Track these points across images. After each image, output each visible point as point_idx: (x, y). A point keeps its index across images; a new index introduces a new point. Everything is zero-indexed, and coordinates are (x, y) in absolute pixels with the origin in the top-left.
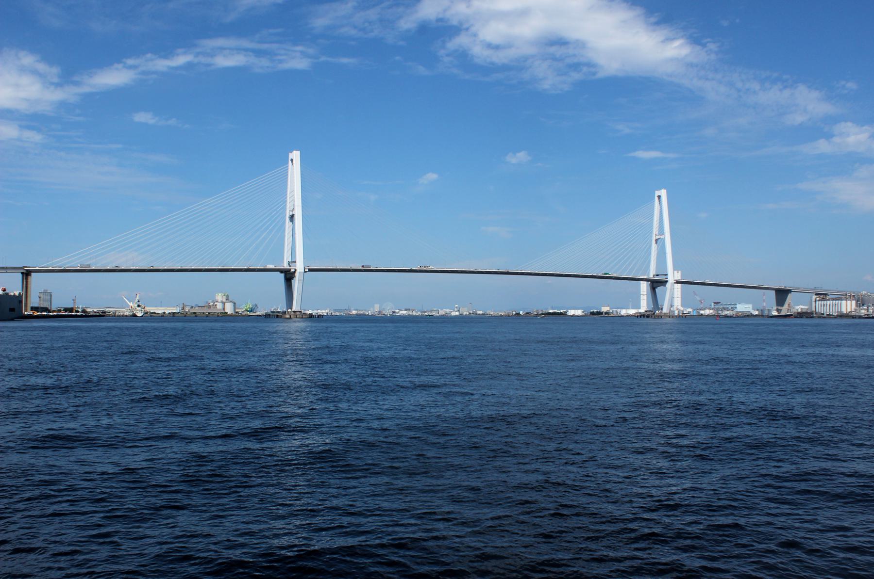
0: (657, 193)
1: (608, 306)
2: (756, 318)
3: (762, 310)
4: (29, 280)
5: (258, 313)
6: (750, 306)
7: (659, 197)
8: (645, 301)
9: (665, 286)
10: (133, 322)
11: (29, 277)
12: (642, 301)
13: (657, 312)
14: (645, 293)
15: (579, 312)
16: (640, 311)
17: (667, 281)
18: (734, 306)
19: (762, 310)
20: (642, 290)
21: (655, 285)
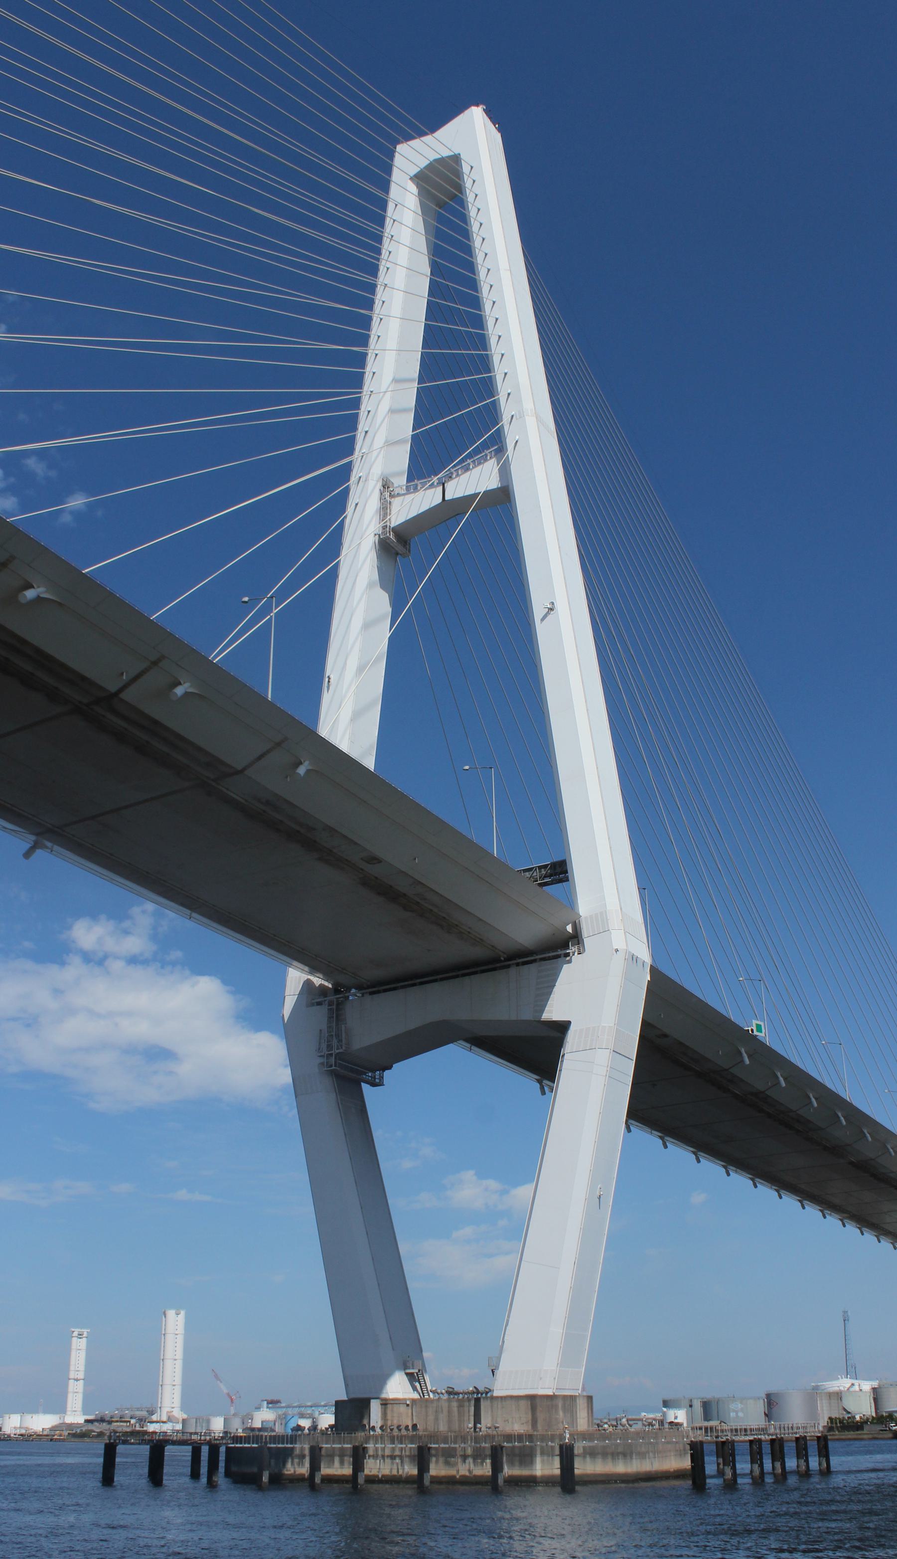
3: (706, 1405)
8: (83, 1355)
12: (70, 1396)
14: (81, 1375)
20: (72, 1368)
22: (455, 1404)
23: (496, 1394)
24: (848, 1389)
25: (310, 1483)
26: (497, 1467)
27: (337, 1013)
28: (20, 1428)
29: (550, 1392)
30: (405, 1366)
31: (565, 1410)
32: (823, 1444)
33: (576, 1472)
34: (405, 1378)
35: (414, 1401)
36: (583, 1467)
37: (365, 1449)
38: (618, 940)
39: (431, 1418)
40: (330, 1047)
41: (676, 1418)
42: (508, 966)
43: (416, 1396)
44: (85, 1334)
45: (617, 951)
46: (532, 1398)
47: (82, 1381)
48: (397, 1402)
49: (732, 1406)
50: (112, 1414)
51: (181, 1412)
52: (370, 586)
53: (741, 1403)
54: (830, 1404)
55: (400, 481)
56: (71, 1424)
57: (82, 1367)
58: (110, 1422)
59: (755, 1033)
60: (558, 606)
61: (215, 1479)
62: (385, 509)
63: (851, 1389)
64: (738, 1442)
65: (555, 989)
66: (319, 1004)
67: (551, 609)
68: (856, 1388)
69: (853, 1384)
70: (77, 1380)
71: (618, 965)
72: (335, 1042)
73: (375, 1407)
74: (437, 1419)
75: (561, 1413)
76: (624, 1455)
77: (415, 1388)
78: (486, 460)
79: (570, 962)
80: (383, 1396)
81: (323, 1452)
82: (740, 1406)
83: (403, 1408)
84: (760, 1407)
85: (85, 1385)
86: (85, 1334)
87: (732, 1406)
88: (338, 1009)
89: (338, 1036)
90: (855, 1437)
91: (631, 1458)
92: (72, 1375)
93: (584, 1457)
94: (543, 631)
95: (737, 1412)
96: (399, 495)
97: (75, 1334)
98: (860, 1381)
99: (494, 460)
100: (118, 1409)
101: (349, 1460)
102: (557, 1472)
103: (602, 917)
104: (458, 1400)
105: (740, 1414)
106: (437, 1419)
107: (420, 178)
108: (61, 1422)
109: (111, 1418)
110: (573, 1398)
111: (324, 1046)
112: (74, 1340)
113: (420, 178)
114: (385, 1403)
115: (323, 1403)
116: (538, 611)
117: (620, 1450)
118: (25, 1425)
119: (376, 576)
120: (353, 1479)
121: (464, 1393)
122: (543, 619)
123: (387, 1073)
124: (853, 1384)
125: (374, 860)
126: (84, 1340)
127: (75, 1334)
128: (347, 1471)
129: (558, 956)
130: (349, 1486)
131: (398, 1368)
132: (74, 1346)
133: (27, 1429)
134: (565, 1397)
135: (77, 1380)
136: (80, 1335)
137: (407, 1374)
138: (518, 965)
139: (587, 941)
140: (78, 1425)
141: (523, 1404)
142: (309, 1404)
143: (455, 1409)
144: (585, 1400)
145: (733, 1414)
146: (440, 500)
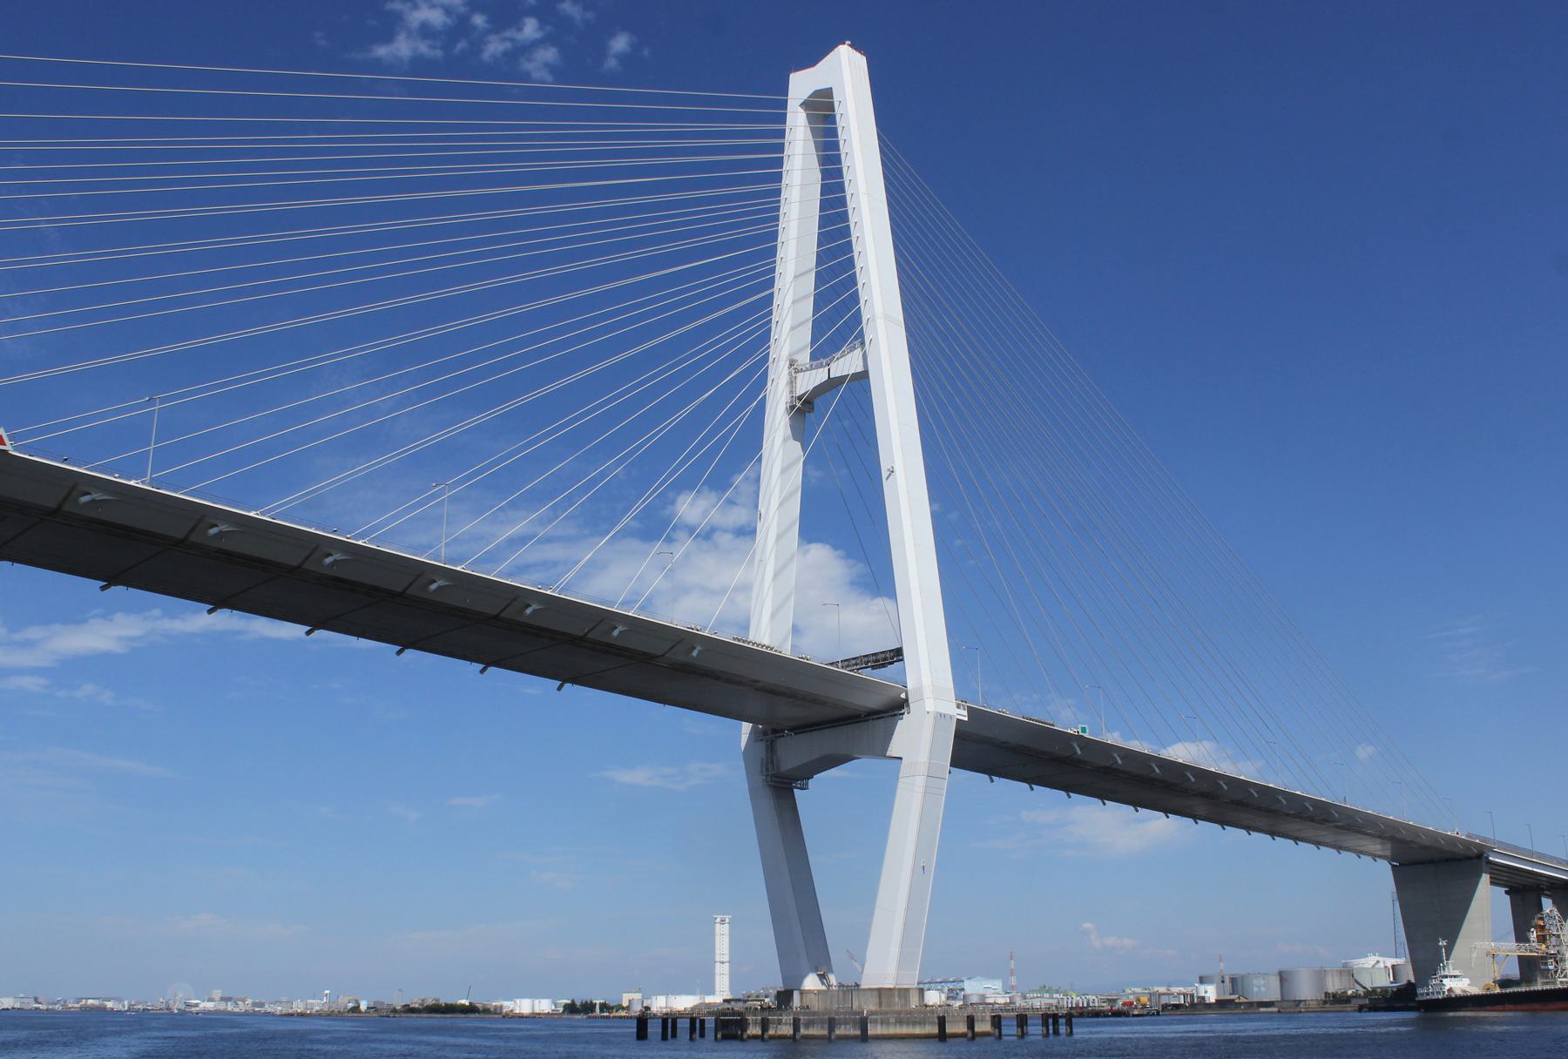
0: (802, 84)
1: (639, 991)
2: (1212, 1015)
3: (1233, 981)
4: (934, 1040)
5: (869, 1025)
6: (997, 985)
7: (822, 109)
8: (726, 939)
9: (879, 749)
10: (1494, 1011)
11: (937, 1040)
12: (717, 978)
13: (811, 982)
14: (726, 958)
15: (545, 1006)
16: (709, 999)
17: (897, 707)
18: (959, 986)
19: (1233, 981)
20: (717, 951)
21: (793, 753)
22: (841, 993)
23: (862, 987)
24: (1374, 966)
25: (761, 1038)
26: (831, 1030)
27: (771, 749)
28: (666, 1007)
29: (892, 987)
30: (816, 970)
31: (899, 997)
32: (1069, 1017)
33: (947, 1031)
34: (817, 978)
35: (819, 991)
36: (949, 1029)
37: (799, 1020)
38: (930, 705)
39: (828, 1003)
40: (767, 770)
41: (1206, 992)
42: (868, 720)
43: (824, 988)
44: (727, 921)
45: (928, 712)
46: (879, 990)
47: (727, 964)
48: (809, 992)
49: (1255, 982)
50: (758, 993)
51: (773, 992)
52: (785, 440)
53: (1264, 979)
54: (1341, 980)
55: (804, 358)
56: (710, 1004)
57: (726, 951)
58: (745, 1001)
59: (1081, 734)
60: (896, 469)
61: (694, 1036)
62: (792, 382)
63: (1377, 966)
64: (1005, 1018)
65: (894, 736)
66: (761, 740)
67: (892, 472)
68: (1381, 965)
69: (1378, 962)
70: (723, 963)
71: (929, 722)
72: (770, 767)
73: (796, 995)
74: (831, 1002)
75: (897, 999)
76: (920, 1024)
77: (823, 983)
78: (855, 349)
79: (902, 719)
80: (802, 988)
81: (802, 1022)
82: (1262, 982)
83: (812, 996)
84: (1275, 982)
85: (730, 967)
86: (727, 921)
87: (1255, 982)
88: (771, 744)
89: (772, 763)
90: (1340, 1009)
91: (925, 1025)
92: (718, 958)
93: (896, 1025)
94: (887, 486)
95: (1259, 987)
96: (802, 371)
97: (718, 920)
98: (1385, 959)
99: (859, 349)
100: (763, 989)
101: (826, 1026)
102: (937, 1031)
103: (920, 690)
104: (843, 991)
105: (1263, 989)
106: (831, 1002)
107: (806, 105)
108: (701, 1001)
109: (749, 997)
110: (907, 990)
111: (764, 769)
112: (718, 926)
113: (806, 105)
114: (802, 993)
115: (951, 980)
116: (884, 474)
117: (917, 1020)
118: (669, 1005)
119: (789, 431)
120: (793, 1037)
121: (847, 986)
122: (887, 479)
123: (810, 781)
124: (1378, 962)
125: (756, 681)
126: (727, 925)
127: (718, 920)
128: (825, 1032)
129: (895, 715)
130: (791, 1041)
131: (812, 972)
132: (717, 932)
133: (671, 1008)
134: (900, 989)
135: (723, 963)
136: (723, 921)
137: (818, 975)
138: (873, 719)
139: (911, 705)
140: (715, 1005)
141: (875, 993)
142: (939, 980)
143: (841, 996)
144: (917, 992)
145: (1255, 989)
146: (827, 378)
